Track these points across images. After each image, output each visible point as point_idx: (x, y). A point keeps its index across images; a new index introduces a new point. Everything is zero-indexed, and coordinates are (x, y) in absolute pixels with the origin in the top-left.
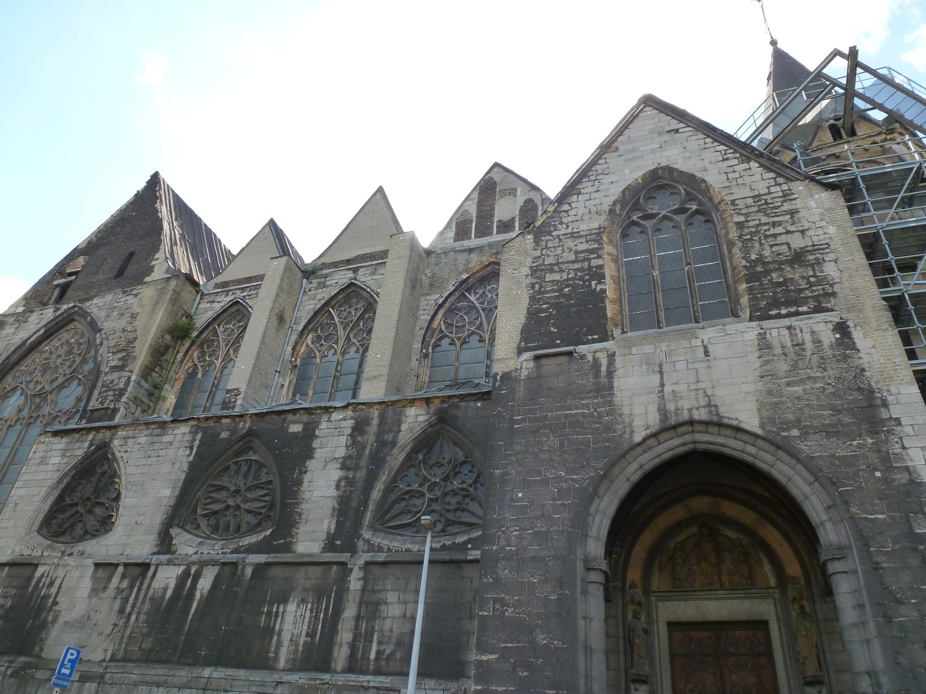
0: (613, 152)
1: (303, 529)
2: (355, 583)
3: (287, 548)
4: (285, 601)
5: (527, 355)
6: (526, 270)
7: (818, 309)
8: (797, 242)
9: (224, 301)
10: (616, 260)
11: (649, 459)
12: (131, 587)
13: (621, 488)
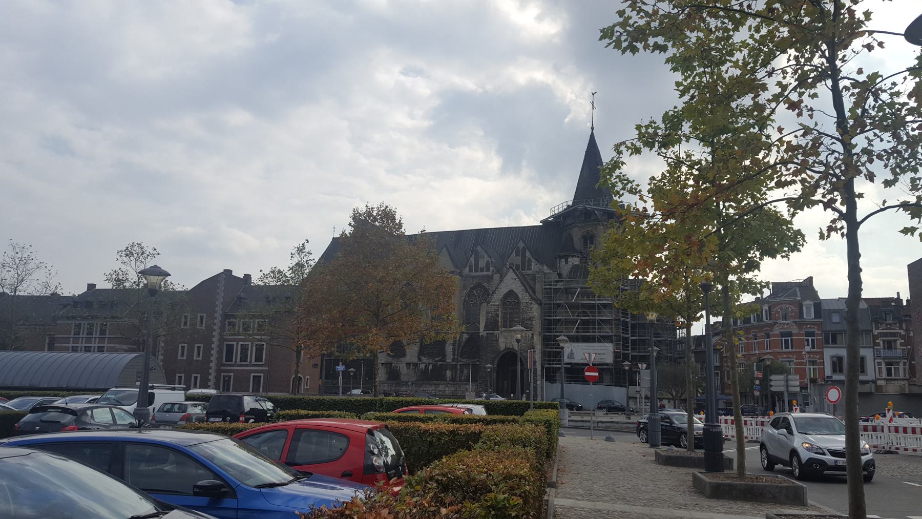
0: (501, 281)
2: (458, 367)
3: (445, 361)
4: (447, 370)
5: (485, 332)
6: (485, 312)
7: (530, 330)
12: (415, 368)
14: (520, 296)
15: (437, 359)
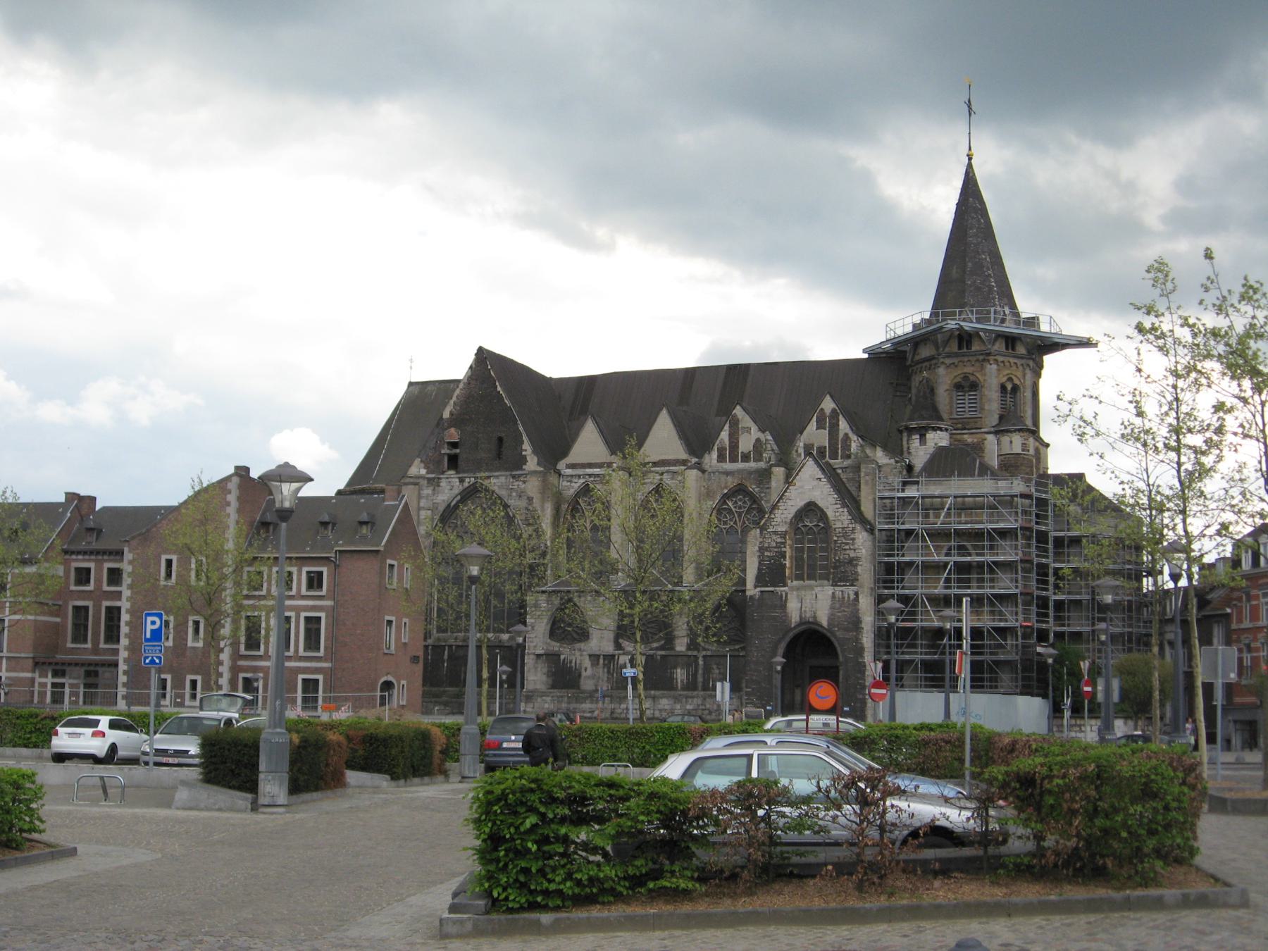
1: (677, 642)
3: (672, 648)
5: (759, 589)
6: (757, 548)
7: (852, 585)
8: (852, 554)
9: (577, 485)
10: (791, 547)
11: (796, 631)
13: (788, 639)
14: (830, 514)
15: (655, 645)
